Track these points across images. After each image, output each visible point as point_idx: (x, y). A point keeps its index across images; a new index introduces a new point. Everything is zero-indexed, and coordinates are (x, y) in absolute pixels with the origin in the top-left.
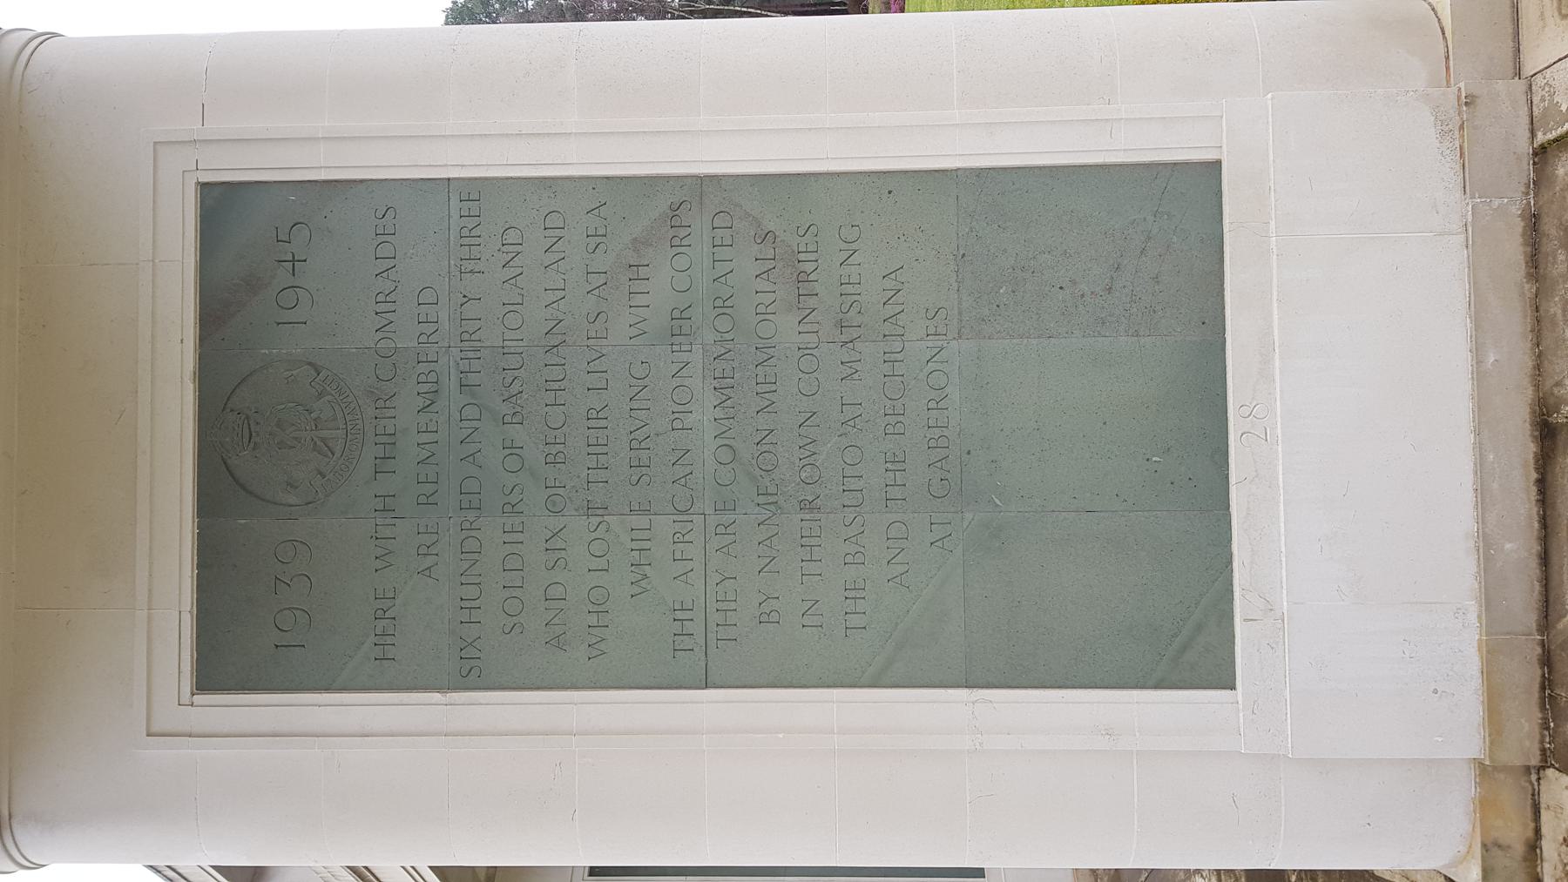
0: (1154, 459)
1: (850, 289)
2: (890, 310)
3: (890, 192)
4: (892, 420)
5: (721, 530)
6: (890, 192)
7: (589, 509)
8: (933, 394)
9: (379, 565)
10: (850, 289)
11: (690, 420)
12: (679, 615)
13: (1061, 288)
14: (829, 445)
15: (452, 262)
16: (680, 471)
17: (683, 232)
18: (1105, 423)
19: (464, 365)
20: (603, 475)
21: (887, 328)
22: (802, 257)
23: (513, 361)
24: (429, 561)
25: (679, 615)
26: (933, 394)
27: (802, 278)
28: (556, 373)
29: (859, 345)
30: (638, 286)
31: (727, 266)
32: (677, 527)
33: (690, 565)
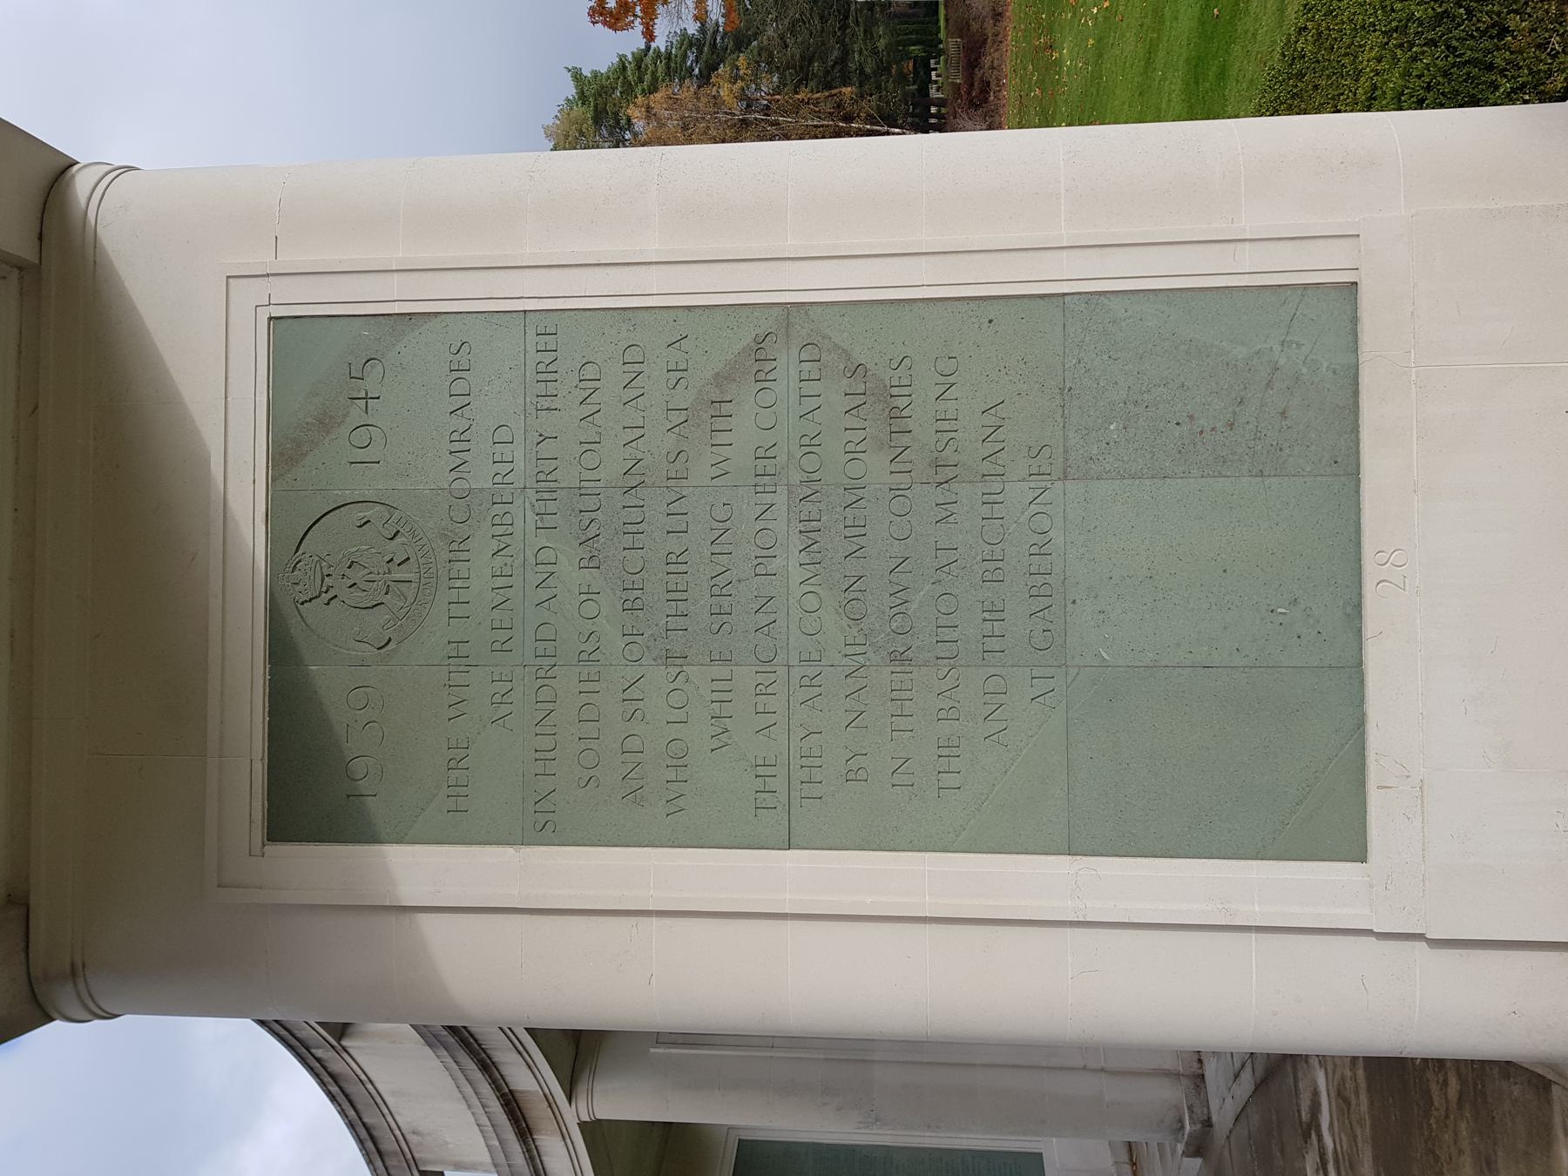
0: (1279, 610)
1: (946, 425)
2: (990, 448)
3: (990, 321)
4: (991, 565)
5: (806, 681)
6: (990, 321)
7: (668, 658)
8: (1036, 538)
9: (452, 712)
10: (946, 425)
11: (773, 566)
12: (761, 771)
13: (1178, 424)
14: (922, 593)
15: (528, 399)
16: (763, 619)
17: (768, 366)
18: (1225, 571)
19: (540, 507)
20: (681, 622)
21: (986, 467)
22: (895, 391)
23: (591, 503)
24: (504, 709)
25: (761, 771)
26: (1036, 538)
27: (895, 414)
28: (635, 515)
29: (954, 486)
30: (720, 424)
31: (815, 402)
32: (760, 678)
33: (772, 719)
